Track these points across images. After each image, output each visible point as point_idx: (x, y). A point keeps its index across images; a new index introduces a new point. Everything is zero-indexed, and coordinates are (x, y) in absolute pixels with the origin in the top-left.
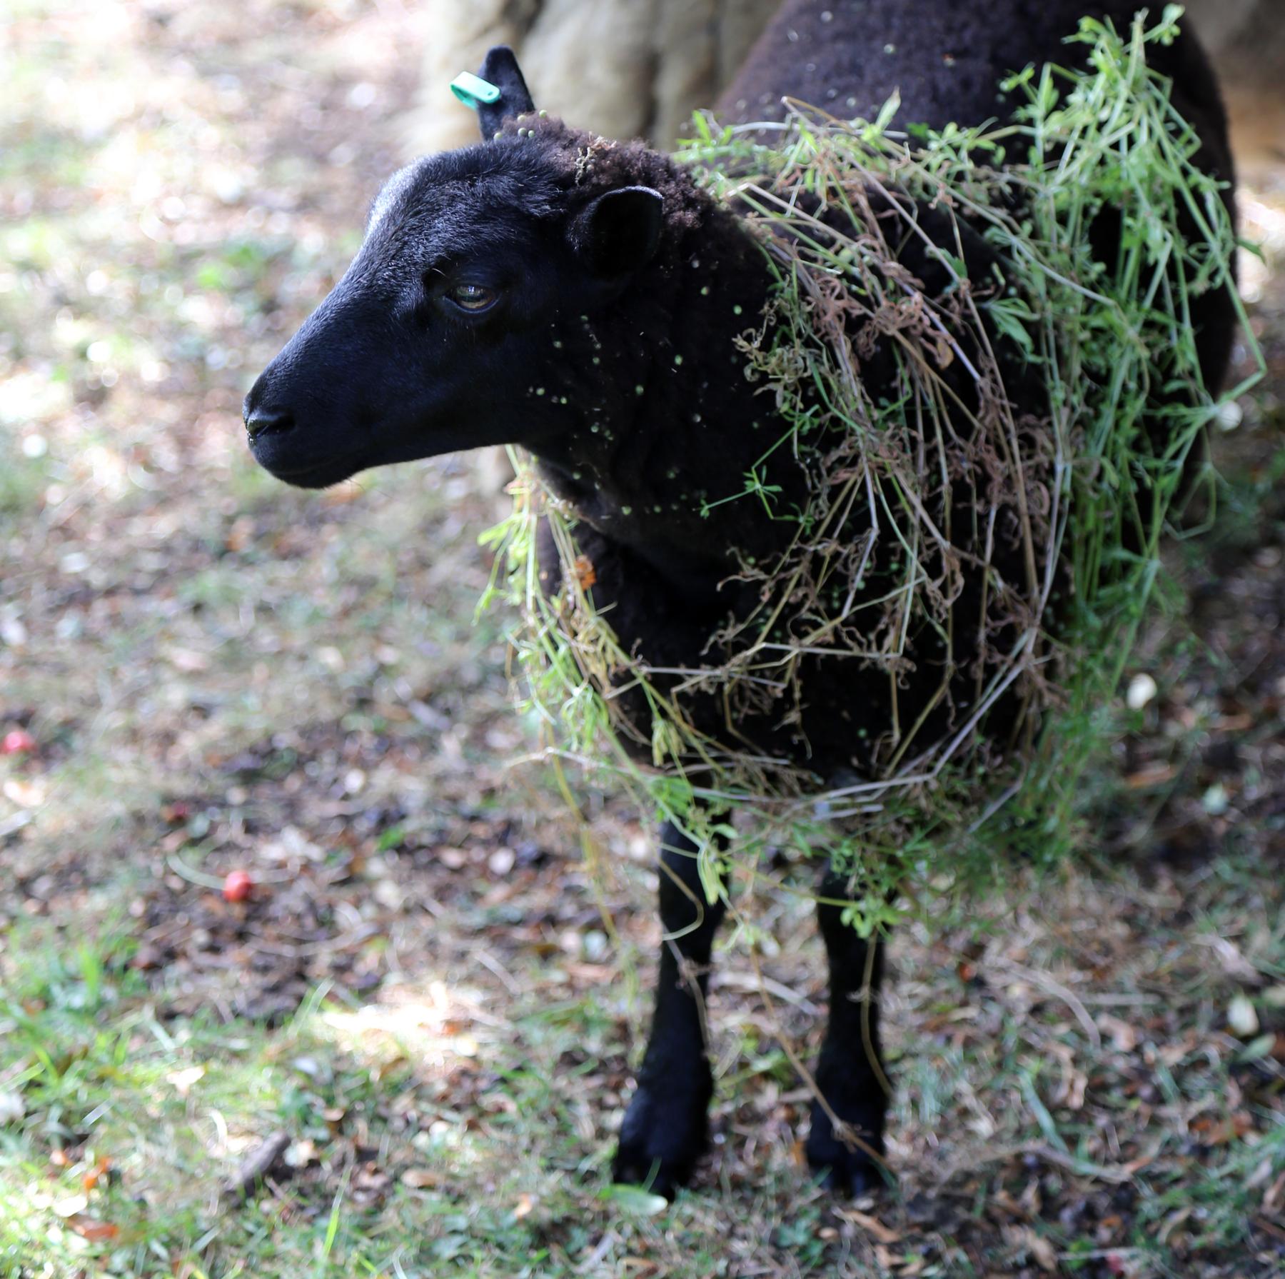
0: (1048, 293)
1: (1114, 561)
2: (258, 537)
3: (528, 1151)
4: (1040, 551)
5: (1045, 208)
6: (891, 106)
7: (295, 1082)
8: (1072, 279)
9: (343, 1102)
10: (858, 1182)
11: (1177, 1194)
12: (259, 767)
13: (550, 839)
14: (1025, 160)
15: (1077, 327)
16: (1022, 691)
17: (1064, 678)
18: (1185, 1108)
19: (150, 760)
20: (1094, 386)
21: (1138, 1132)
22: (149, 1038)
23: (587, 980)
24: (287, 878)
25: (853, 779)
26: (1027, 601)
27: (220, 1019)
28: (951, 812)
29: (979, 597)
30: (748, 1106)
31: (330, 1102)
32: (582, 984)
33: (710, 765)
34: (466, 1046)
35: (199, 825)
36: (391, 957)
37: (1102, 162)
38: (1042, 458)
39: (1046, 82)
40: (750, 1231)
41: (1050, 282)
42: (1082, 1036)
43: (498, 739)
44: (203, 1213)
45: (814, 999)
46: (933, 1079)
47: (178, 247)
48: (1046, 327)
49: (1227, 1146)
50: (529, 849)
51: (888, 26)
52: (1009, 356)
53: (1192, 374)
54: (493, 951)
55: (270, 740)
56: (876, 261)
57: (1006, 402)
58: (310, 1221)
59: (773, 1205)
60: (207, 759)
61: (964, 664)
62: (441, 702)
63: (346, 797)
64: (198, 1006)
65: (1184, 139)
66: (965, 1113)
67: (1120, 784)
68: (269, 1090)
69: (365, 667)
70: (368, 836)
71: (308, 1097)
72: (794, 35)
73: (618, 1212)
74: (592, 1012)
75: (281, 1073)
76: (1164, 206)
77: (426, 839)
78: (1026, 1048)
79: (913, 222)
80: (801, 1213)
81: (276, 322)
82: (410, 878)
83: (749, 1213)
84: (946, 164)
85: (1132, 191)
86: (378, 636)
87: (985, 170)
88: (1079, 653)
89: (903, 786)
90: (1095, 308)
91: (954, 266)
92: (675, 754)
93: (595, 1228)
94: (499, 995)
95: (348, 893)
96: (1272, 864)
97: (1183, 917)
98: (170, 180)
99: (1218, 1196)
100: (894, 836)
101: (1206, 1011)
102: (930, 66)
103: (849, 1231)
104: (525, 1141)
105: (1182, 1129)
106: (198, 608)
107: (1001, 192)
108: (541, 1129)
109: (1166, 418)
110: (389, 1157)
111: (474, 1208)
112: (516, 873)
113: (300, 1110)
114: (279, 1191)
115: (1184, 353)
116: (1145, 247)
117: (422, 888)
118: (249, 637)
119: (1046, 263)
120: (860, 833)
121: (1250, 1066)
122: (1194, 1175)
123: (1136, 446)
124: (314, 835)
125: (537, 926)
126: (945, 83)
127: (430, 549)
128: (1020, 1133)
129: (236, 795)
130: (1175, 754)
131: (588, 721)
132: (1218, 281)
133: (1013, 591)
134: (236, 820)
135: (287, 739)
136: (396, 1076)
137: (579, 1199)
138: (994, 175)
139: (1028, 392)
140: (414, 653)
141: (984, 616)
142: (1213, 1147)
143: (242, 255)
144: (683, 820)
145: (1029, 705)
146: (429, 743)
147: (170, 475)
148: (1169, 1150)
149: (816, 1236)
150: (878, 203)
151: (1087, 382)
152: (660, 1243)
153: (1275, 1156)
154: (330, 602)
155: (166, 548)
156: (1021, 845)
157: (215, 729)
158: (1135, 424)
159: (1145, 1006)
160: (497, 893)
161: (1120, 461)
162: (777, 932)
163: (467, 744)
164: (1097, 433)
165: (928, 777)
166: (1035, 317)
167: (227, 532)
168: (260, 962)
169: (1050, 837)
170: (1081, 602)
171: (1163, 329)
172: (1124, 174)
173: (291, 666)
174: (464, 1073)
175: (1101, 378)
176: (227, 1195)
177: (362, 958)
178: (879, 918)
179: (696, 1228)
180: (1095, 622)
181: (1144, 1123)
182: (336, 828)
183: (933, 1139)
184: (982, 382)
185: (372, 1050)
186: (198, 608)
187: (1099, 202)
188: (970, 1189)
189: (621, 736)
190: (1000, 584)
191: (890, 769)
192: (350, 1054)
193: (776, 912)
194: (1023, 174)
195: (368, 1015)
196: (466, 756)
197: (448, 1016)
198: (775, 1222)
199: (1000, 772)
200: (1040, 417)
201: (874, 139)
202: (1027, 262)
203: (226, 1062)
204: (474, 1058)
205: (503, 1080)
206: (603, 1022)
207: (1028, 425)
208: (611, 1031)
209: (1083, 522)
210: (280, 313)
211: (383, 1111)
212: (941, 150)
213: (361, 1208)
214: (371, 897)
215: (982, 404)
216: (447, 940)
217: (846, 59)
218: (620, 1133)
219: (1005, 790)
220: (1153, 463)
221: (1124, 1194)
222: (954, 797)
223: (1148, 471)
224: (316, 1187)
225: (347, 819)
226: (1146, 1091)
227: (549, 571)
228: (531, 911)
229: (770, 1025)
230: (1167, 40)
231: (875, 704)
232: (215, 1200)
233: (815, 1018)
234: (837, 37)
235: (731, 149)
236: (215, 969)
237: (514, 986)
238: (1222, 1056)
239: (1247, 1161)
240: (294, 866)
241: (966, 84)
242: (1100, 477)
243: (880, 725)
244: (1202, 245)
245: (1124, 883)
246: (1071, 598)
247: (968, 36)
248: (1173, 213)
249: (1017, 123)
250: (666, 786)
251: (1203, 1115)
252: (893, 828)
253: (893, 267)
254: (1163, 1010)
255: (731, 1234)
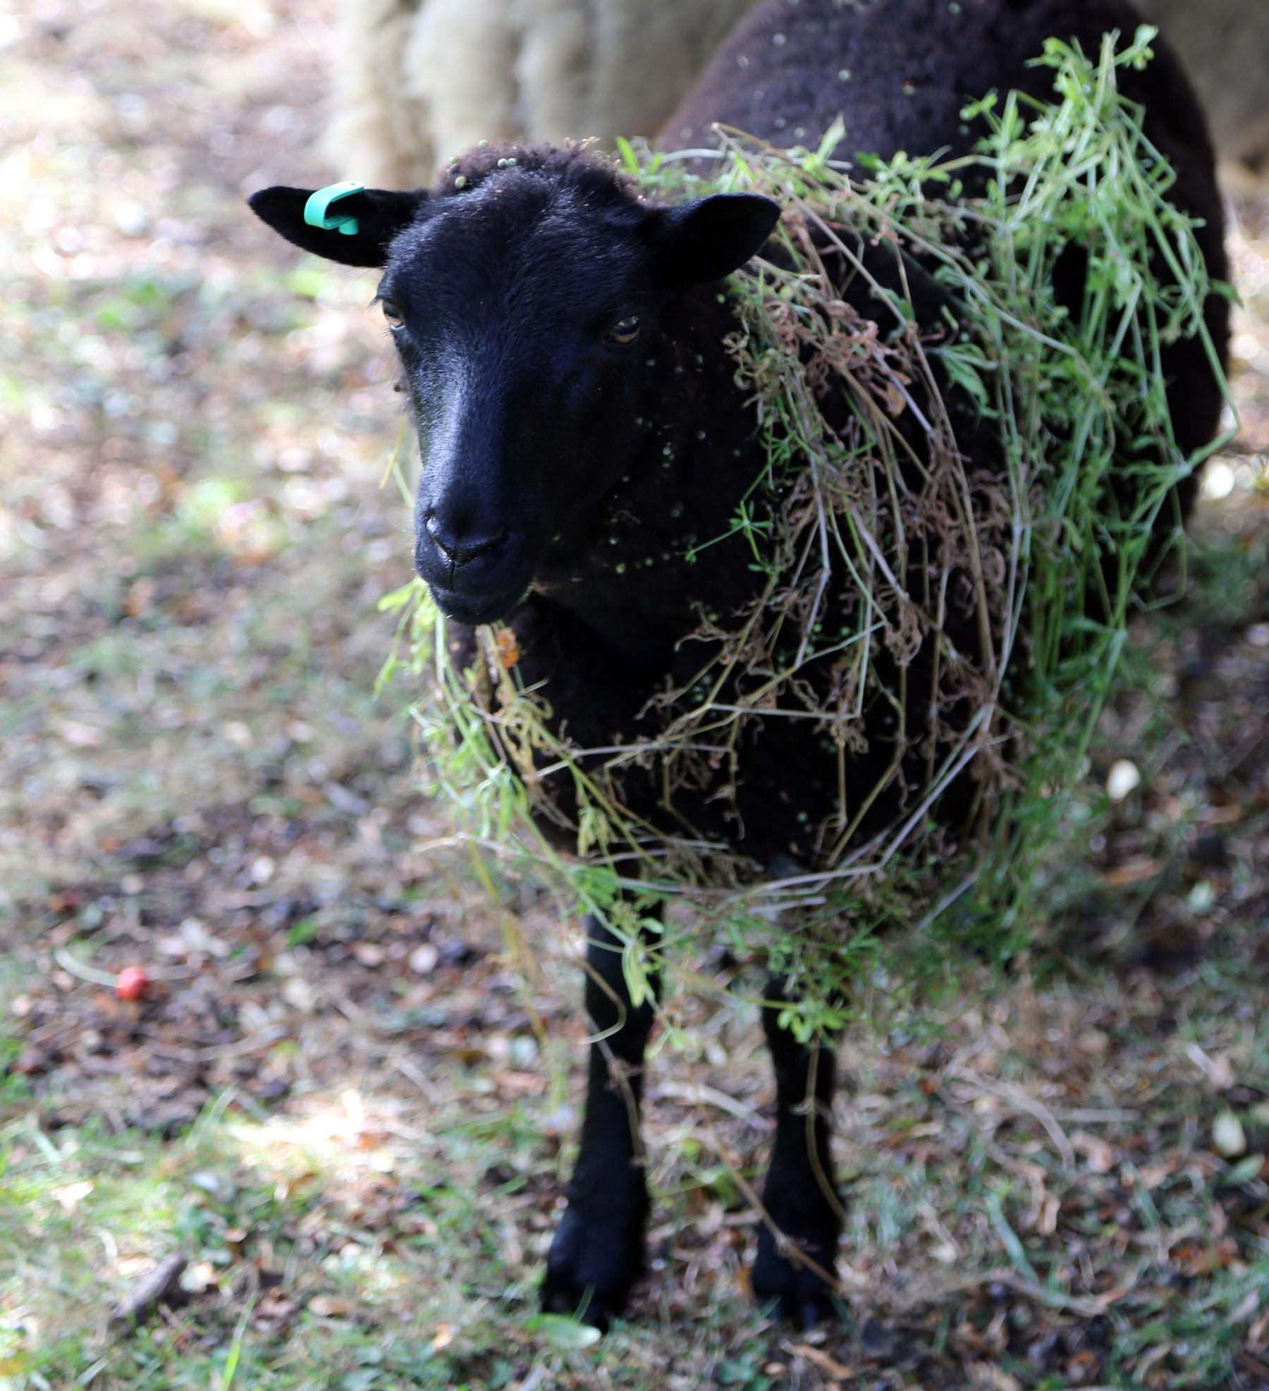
0: (1004, 339)
1: (1076, 632)
2: (160, 601)
3: (449, 1277)
4: (996, 621)
5: (1003, 246)
6: (836, 133)
7: (194, 1199)
8: (1032, 325)
9: (245, 1221)
10: (809, 1312)
11: (1156, 1328)
12: (157, 853)
13: (475, 936)
14: (983, 194)
15: (1037, 376)
16: (978, 774)
17: (1022, 758)
18: (1165, 1234)
19: (37, 843)
20: (1055, 440)
21: (1114, 1260)
22: (32, 1149)
23: (516, 1090)
24: (186, 975)
25: (794, 869)
26: (983, 674)
27: (110, 1128)
28: (899, 906)
29: (930, 669)
30: (690, 1229)
31: (231, 1221)
32: (511, 1094)
33: (639, 853)
34: (382, 1161)
35: (91, 915)
36: (301, 1062)
37: (1068, 195)
38: (997, 520)
39: (1011, 110)
40: (690, 1365)
41: (1006, 327)
42: (1055, 1155)
43: (420, 824)
44: (89, 1342)
45: (762, 1112)
46: (892, 1201)
47: (75, 283)
48: (1002, 377)
49: (1210, 1276)
50: (453, 945)
51: (845, 49)
52: (961, 407)
53: (1162, 429)
54: (411, 1057)
55: (170, 822)
56: (820, 300)
57: (958, 456)
58: (208, 1352)
59: (716, 1338)
60: (100, 844)
61: (917, 741)
62: (358, 784)
63: (253, 887)
64: (87, 1115)
65: (1157, 172)
66: (927, 1239)
67: (1099, 881)
68: (164, 1207)
69: (275, 744)
70: (277, 929)
71: (207, 1216)
72: (744, 61)
73: (547, 1344)
74: (520, 1125)
75: (177, 1189)
76: (1134, 245)
77: (341, 933)
78: (994, 1167)
79: (858, 263)
80: (746, 1347)
81: (181, 365)
82: (322, 976)
83: (690, 1346)
84: (895, 197)
85: (1100, 229)
86: (290, 710)
87: (938, 205)
88: (1039, 731)
89: (848, 878)
90: (1056, 356)
91: (899, 305)
92: (604, 843)
93: (521, 1361)
94: (418, 1106)
95: (253, 992)
96: (1259, 972)
97: (1166, 1025)
98: (65, 208)
99: (1200, 1331)
100: (837, 932)
101: (1190, 1130)
102: (888, 95)
103: (798, 1366)
104: (445, 1266)
105: (1162, 1257)
106: (92, 678)
107: (956, 229)
108: (463, 1253)
109: (1134, 477)
110: (295, 1282)
111: (389, 1338)
112: (439, 972)
113: (199, 1230)
114: (174, 1319)
115: (1154, 406)
116: (1112, 291)
117: (335, 988)
118: (148, 711)
119: (1004, 306)
120: (801, 928)
121: (1236, 1190)
122: (1174, 1308)
123: (1101, 507)
124: (217, 928)
125: (462, 1030)
126: (902, 112)
127: (349, 616)
128: (986, 1261)
129: (132, 884)
130: (1158, 849)
131: (505, 804)
132: (1192, 329)
133: (967, 662)
134: (132, 909)
135: (189, 823)
136: (304, 1193)
137: (504, 1329)
138: (948, 209)
139: (983, 447)
140: (327, 732)
141: (936, 690)
142: (1195, 1278)
143: (146, 291)
144: (608, 913)
145: (986, 788)
146: (345, 829)
147: (62, 531)
148: (1148, 1280)
149: (762, 1372)
150: (820, 239)
151: (1048, 436)
152: (592, 1378)
153: (1262, 1289)
154: (238, 672)
155: (58, 614)
156: (980, 943)
157: (111, 810)
158: (1100, 483)
159: (1124, 1123)
160: (417, 994)
161: (1083, 523)
162: (725, 1039)
163: (387, 830)
164: (1058, 492)
165: (875, 868)
166: (991, 365)
167: (125, 594)
168: (156, 1067)
169: (1005, 934)
170: (1040, 676)
171: (1133, 380)
172: (1092, 210)
173: (194, 742)
174: (379, 1191)
175: (1064, 433)
176: (116, 1323)
177: (268, 1064)
178: (819, 1022)
179: (632, 1363)
180: (1055, 698)
181: (1120, 1251)
182: (242, 921)
183: (891, 1266)
184: (932, 433)
185: (278, 1163)
186: (92, 678)
187: (1062, 241)
188: (930, 1321)
189: (541, 821)
190: (953, 654)
191: (835, 855)
192: (254, 1169)
193: (722, 1017)
194: (981, 209)
195: (276, 1127)
196: (385, 842)
197: (362, 1129)
198: (718, 1356)
199: (954, 861)
200: (995, 474)
201: (817, 170)
202: (982, 305)
203: (117, 1177)
204: (390, 1174)
205: (422, 1199)
206: (532, 1136)
207: (982, 481)
208: (539, 1145)
209: (1042, 588)
210: (186, 356)
211: (289, 1231)
212: (890, 181)
213: (264, 1338)
214: (279, 997)
215: (933, 456)
216: (363, 1045)
217: (796, 87)
218: (549, 1257)
219: (959, 882)
220: (1119, 526)
221: (1098, 1329)
222: (905, 889)
223: (1113, 535)
224: (215, 1315)
225: (254, 911)
226: (1123, 1216)
227: (462, 640)
228: (454, 1014)
229: (709, 1138)
230: (1140, 64)
231: (817, 785)
232: (102, 1328)
233: (764, 1133)
234: (788, 61)
235: (659, 179)
236: (107, 1075)
237: (435, 1095)
238: (1206, 1178)
239: (1231, 1292)
240: (195, 962)
241: (926, 114)
242: (1061, 541)
243: (824, 808)
244: (1174, 288)
245: (1102, 988)
246: (1029, 673)
247: (930, 63)
248: (1146, 254)
249: (981, 153)
250: (589, 876)
251: (1185, 1242)
252: (836, 922)
253: (838, 306)
254: (1143, 1128)
255: (670, 1369)
